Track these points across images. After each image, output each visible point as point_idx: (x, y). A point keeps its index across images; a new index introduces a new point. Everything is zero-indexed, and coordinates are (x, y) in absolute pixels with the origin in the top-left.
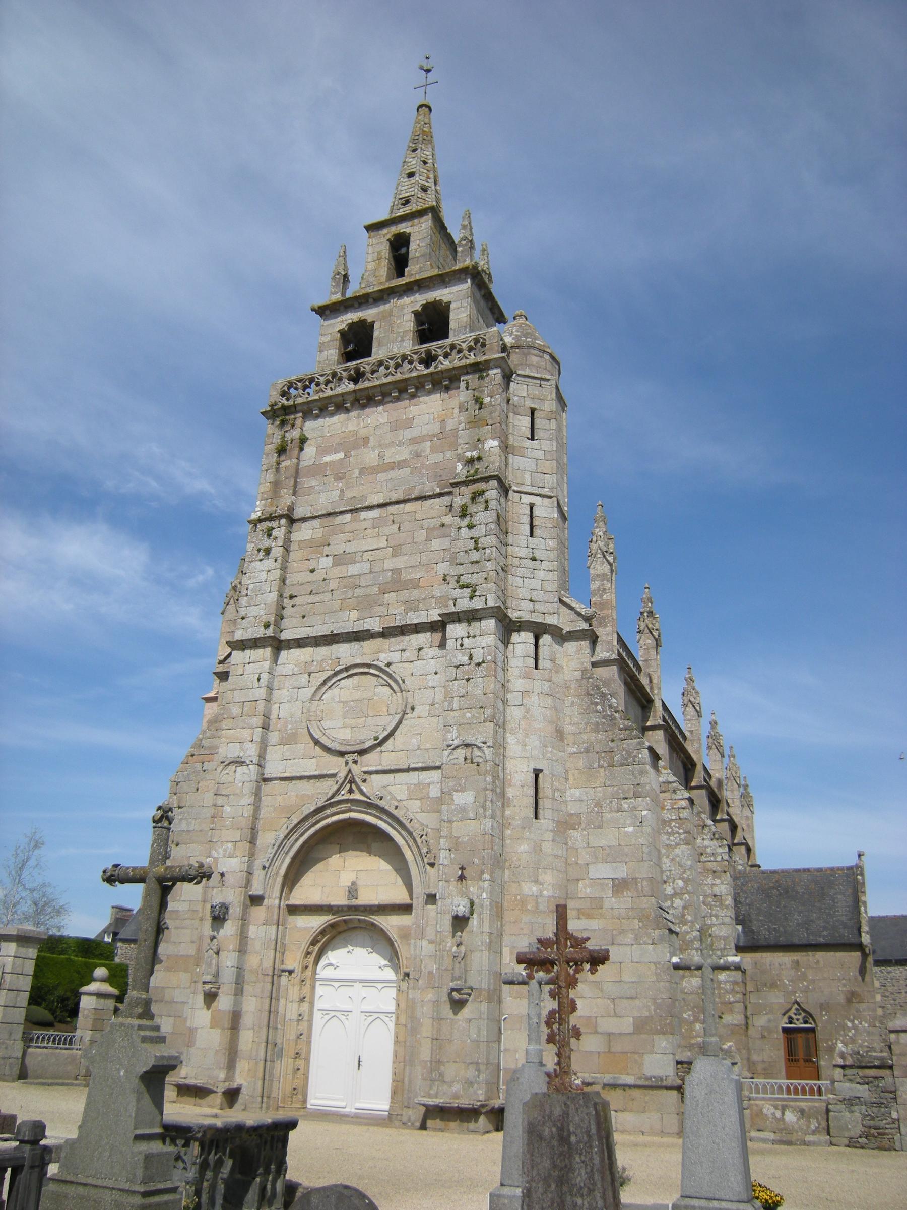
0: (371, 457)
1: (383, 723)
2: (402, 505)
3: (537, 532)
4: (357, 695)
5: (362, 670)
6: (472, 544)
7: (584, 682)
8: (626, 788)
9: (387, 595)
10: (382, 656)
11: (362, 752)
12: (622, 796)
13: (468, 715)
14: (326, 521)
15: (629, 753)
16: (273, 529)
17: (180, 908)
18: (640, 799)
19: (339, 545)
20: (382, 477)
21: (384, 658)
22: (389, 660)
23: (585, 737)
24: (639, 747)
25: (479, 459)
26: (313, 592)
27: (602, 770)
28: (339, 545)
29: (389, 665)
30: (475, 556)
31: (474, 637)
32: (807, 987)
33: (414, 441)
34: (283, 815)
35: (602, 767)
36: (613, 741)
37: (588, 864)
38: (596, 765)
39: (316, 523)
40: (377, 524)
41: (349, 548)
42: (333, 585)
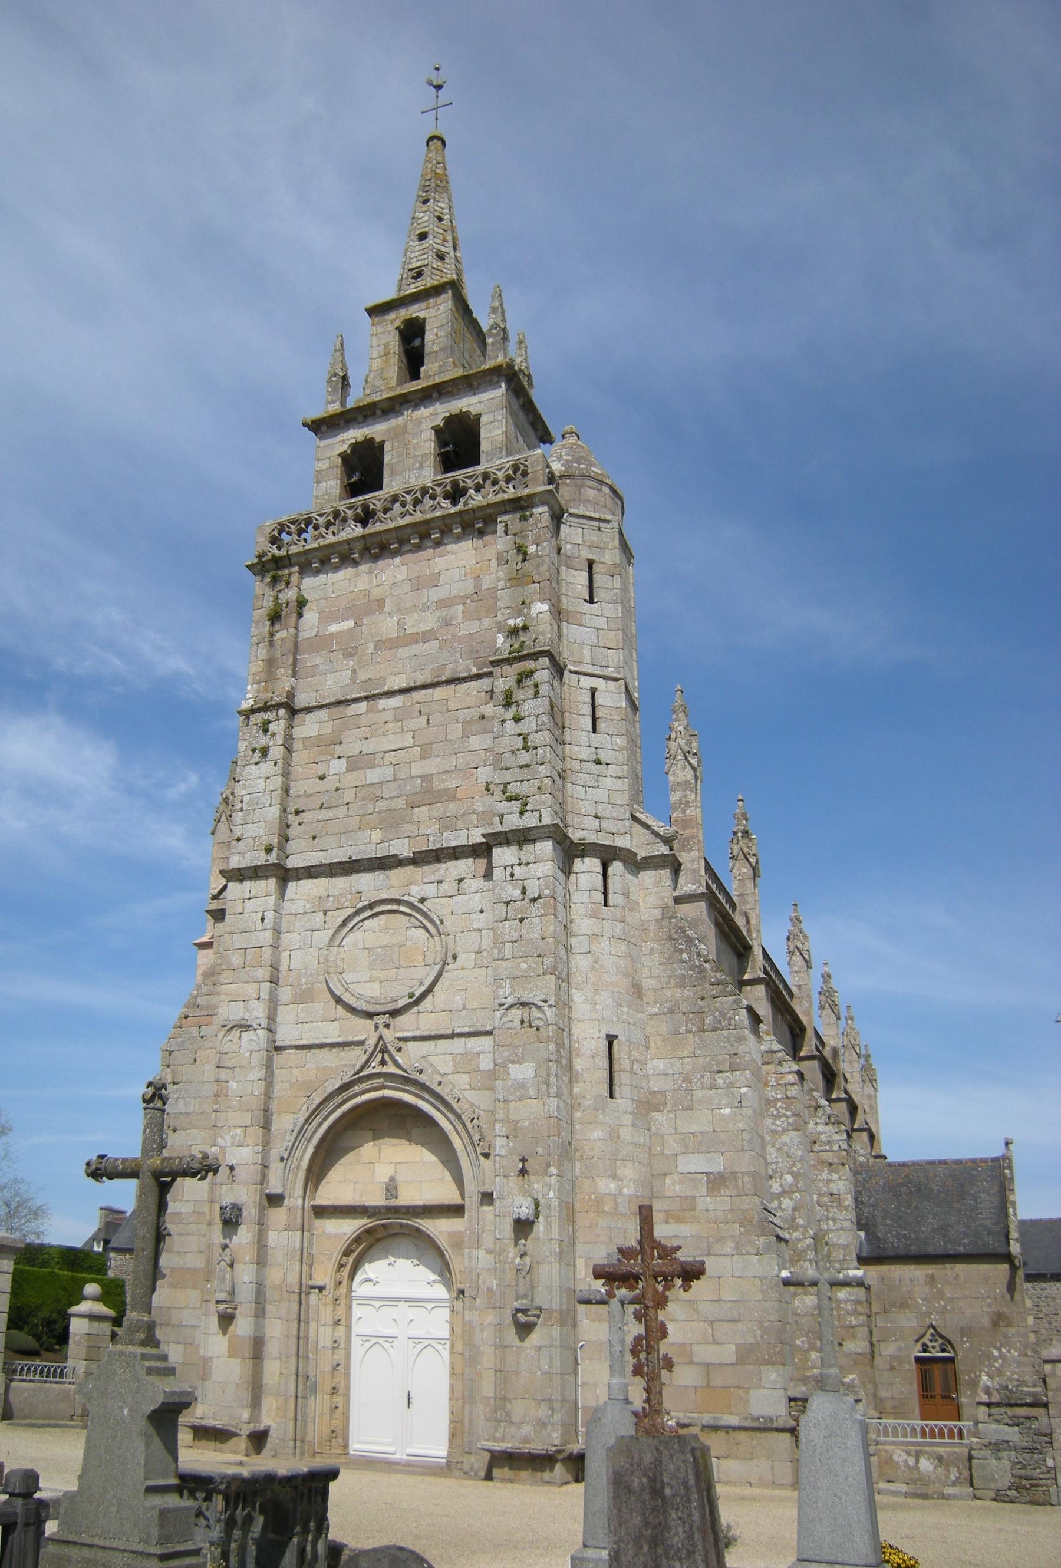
0: (387, 625)
1: (419, 976)
2: (430, 691)
3: (601, 726)
4: (386, 939)
5: (389, 907)
6: (520, 742)
7: (665, 923)
8: (720, 1058)
9: (416, 810)
10: (414, 890)
11: (395, 1013)
12: (715, 1068)
13: (524, 966)
14: (336, 711)
15: (723, 1014)
16: (270, 722)
17: (183, 1210)
18: (738, 1072)
19: (353, 745)
20: (403, 652)
21: (416, 892)
22: (423, 894)
23: (668, 993)
24: (735, 1006)
25: (525, 628)
26: (325, 806)
27: (691, 1036)
28: (353, 745)
29: (423, 900)
30: (524, 757)
31: (528, 864)
32: (945, 1307)
33: (443, 604)
34: (302, 1093)
35: (690, 1032)
36: (702, 999)
37: (676, 1155)
38: (682, 1030)
39: (323, 714)
40: (400, 716)
41: (368, 747)
42: (349, 796)
